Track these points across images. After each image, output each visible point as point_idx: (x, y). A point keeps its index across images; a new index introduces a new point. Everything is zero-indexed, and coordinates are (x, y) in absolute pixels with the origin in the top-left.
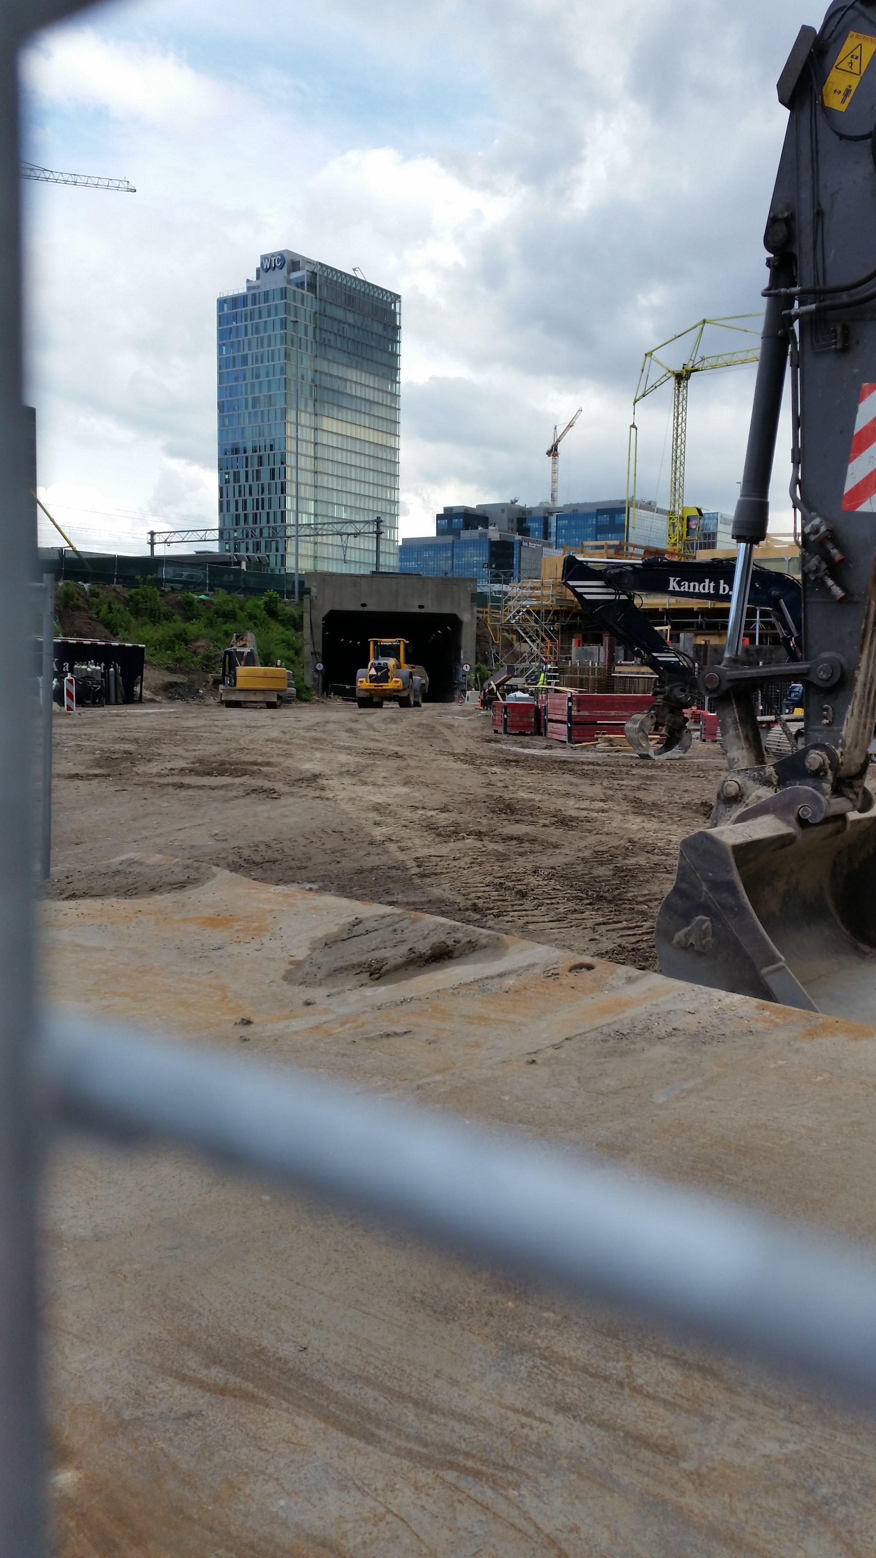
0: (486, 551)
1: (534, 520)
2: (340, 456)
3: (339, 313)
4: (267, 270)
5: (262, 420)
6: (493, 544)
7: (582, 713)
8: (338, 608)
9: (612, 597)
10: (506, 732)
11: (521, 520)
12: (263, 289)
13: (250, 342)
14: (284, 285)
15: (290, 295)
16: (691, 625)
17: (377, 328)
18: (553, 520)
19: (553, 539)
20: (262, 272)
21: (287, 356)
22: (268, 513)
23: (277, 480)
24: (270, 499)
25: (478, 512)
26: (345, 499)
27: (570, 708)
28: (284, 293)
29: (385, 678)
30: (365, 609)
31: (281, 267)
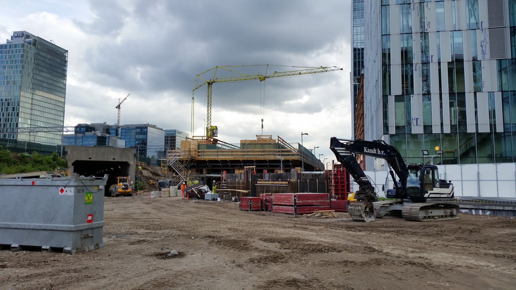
0: (96, 140)
1: (113, 129)
2: (42, 104)
3: (44, 54)
4: (16, 37)
5: (11, 89)
6: (98, 137)
7: (300, 202)
8: (79, 159)
9: (349, 154)
10: (251, 210)
11: (107, 129)
12: (14, 43)
13: (7, 61)
14: (23, 43)
15: (25, 46)
16: (237, 166)
17: (59, 61)
18: (120, 130)
19: (120, 136)
20: (14, 38)
21: (23, 67)
22: (10, 124)
23: (15, 111)
24: (12, 119)
25: (91, 126)
26: (43, 119)
27: (295, 200)
28: (23, 45)
29: (127, 188)
30: (91, 160)
31: (22, 37)
